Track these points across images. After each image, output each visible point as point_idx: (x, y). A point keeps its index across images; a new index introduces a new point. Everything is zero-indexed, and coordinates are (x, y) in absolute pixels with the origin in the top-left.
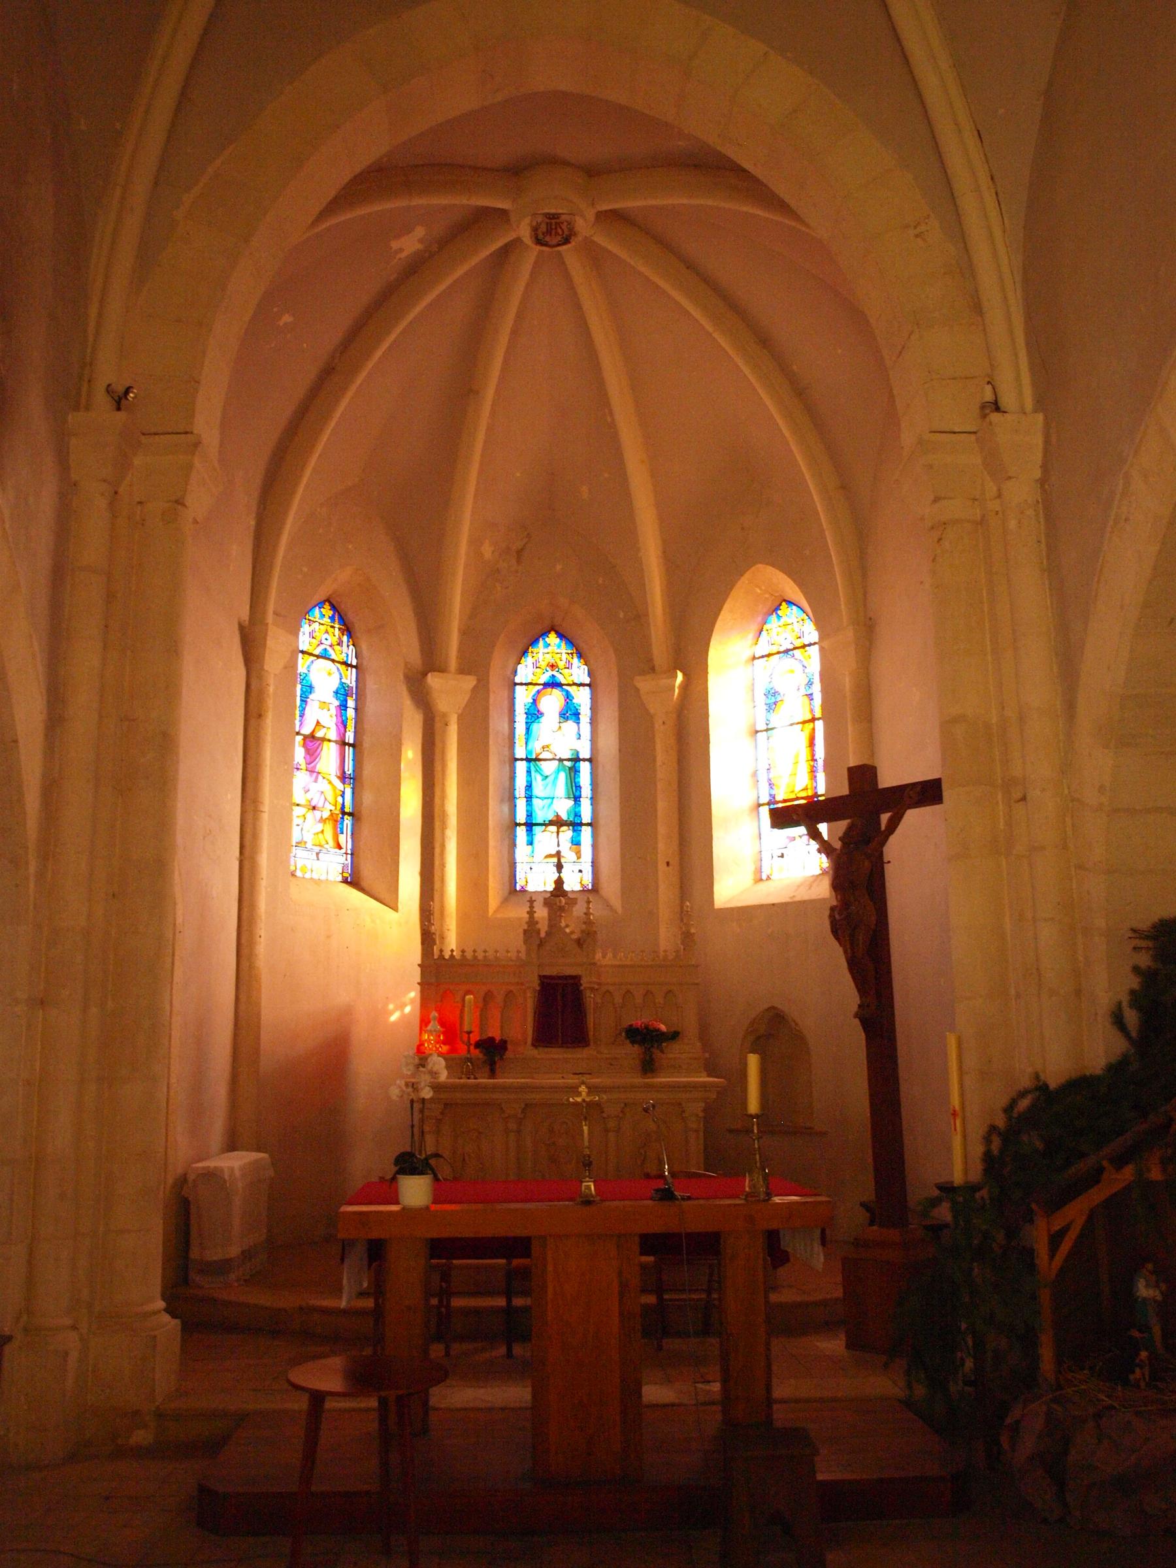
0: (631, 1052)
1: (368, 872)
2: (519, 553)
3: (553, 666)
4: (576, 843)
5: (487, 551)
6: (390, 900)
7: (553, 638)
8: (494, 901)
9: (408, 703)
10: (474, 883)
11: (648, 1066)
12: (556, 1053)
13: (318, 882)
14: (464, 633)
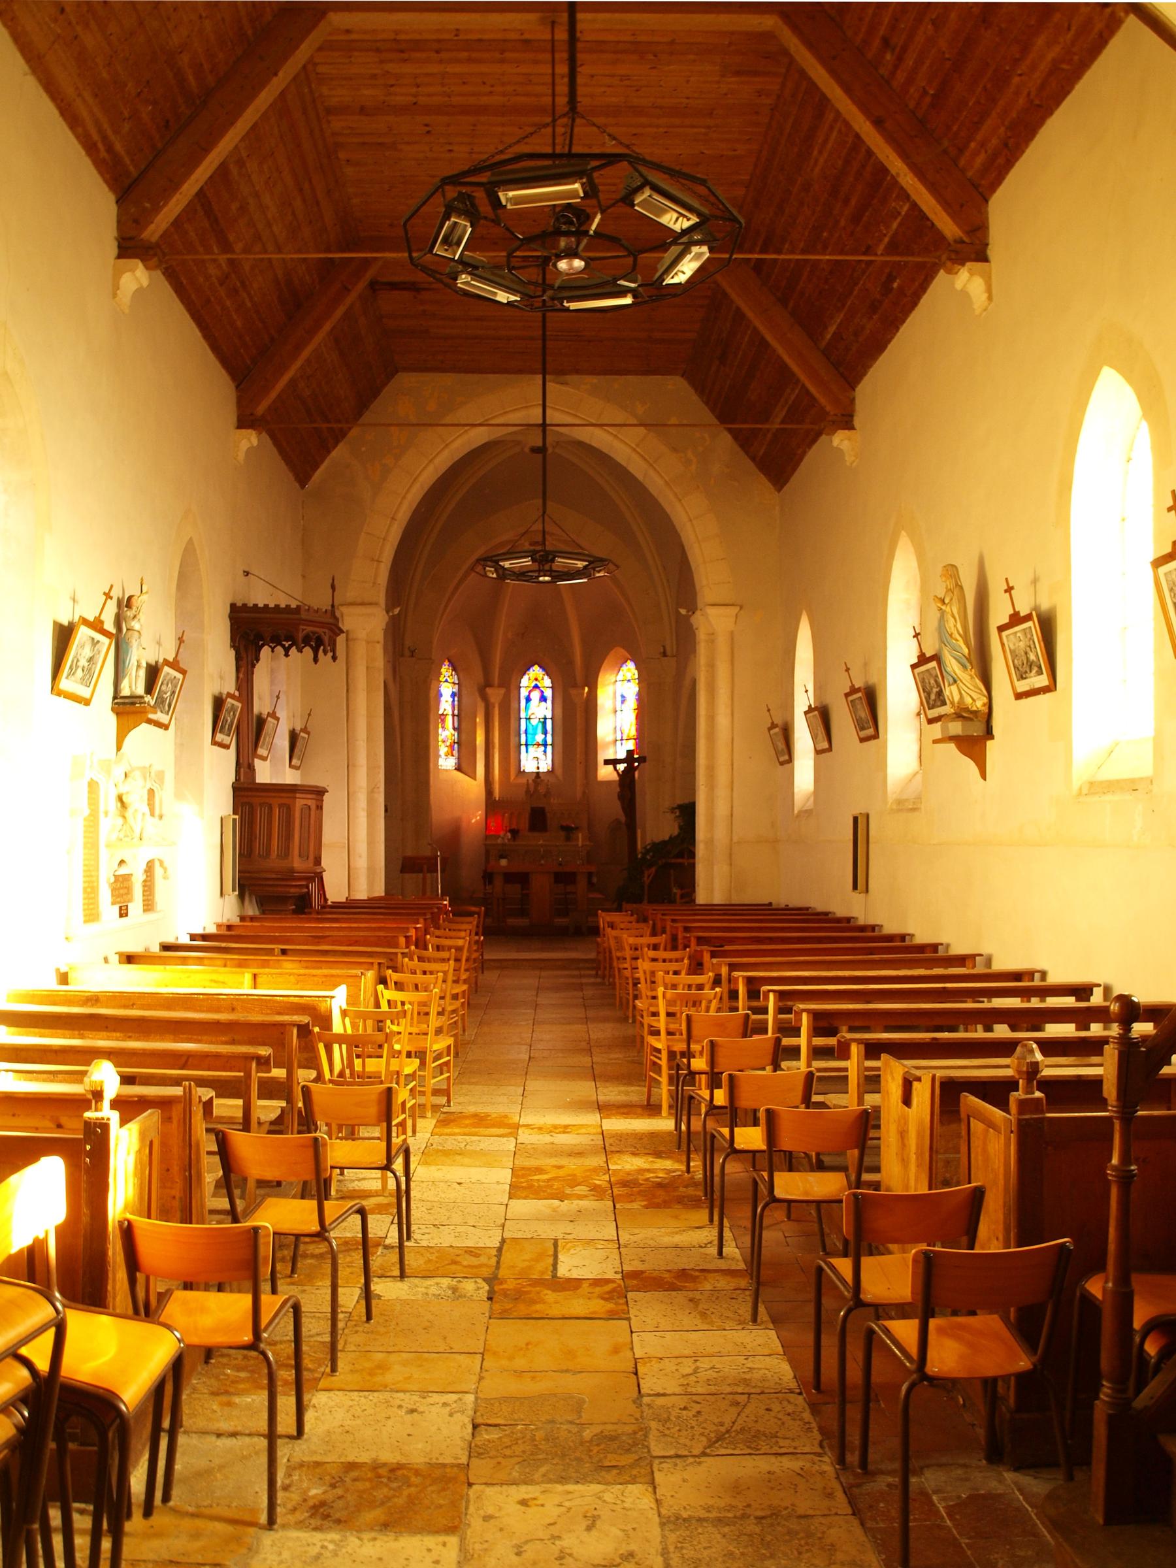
0: (562, 834)
1: (464, 766)
2: (523, 634)
3: (536, 679)
4: (545, 752)
5: (510, 635)
6: (473, 776)
7: (536, 667)
8: (512, 777)
9: (479, 699)
10: (505, 769)
11: (568, 839)
12: (536, 834)
13: (446, 770)
14: (501, 668)
